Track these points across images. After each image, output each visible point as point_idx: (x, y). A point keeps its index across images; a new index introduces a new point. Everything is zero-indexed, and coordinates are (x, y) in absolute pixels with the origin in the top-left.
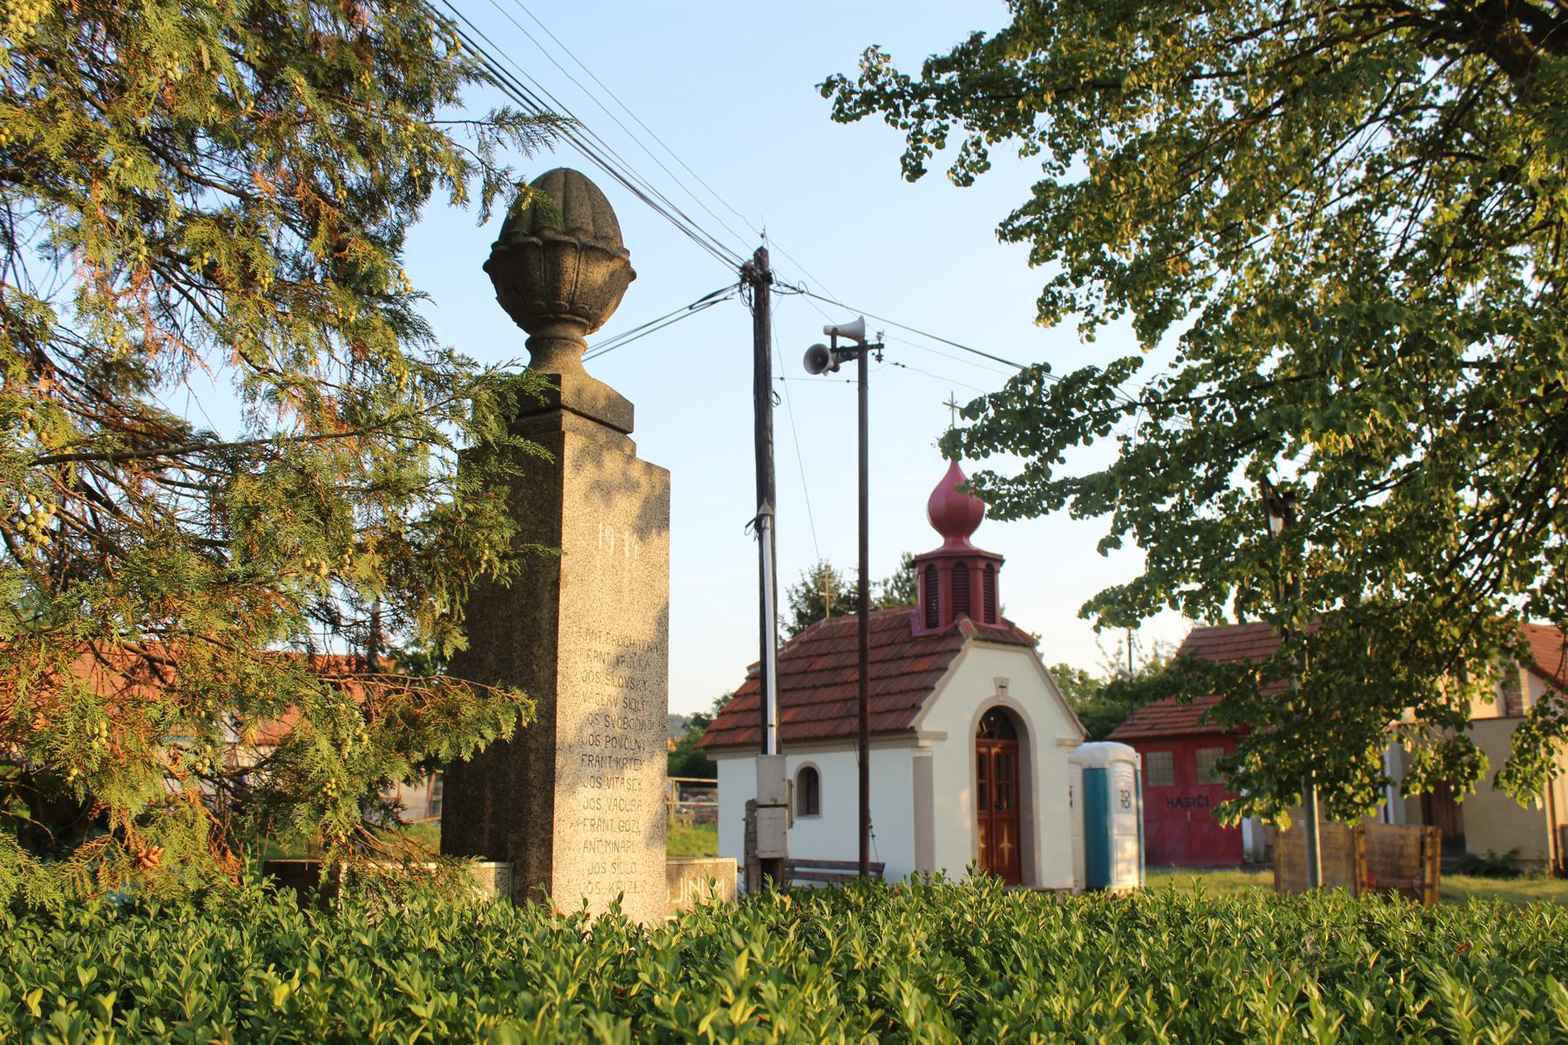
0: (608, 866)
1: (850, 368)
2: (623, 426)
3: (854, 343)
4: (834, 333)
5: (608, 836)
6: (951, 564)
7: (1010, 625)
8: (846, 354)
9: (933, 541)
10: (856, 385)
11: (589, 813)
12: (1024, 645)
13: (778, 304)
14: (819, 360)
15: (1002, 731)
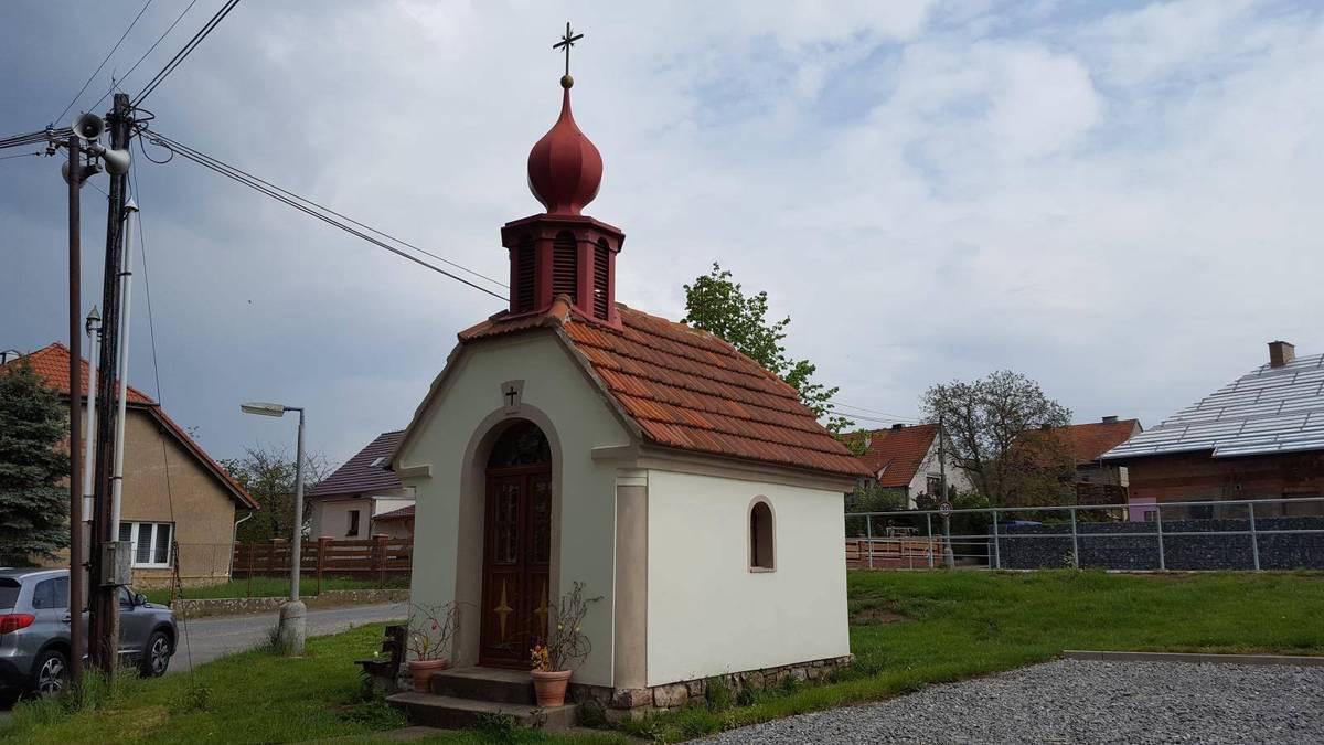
9: (537, 208)
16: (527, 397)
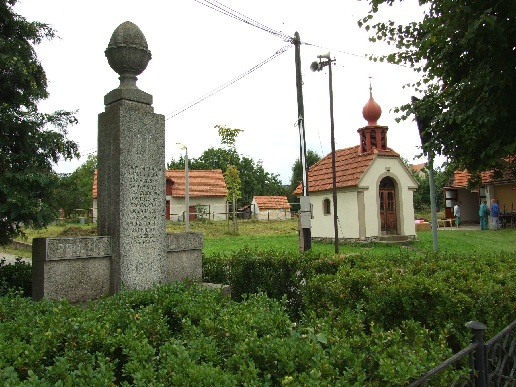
0: (143, 236)
1: (326, 68)
2: (148, 102)
3: (327, 60)
4: (320, 57)
5: (142, 227)
6: (370, 131)
7: (391, 150)
8: (324, 64)
9: (365, 123)
10: (328, 74)
11: (134, 221)
12: (395, 156)
13: (302, 47)
14: (315, 67)
15: (388, 184)
16: (391, 171)
